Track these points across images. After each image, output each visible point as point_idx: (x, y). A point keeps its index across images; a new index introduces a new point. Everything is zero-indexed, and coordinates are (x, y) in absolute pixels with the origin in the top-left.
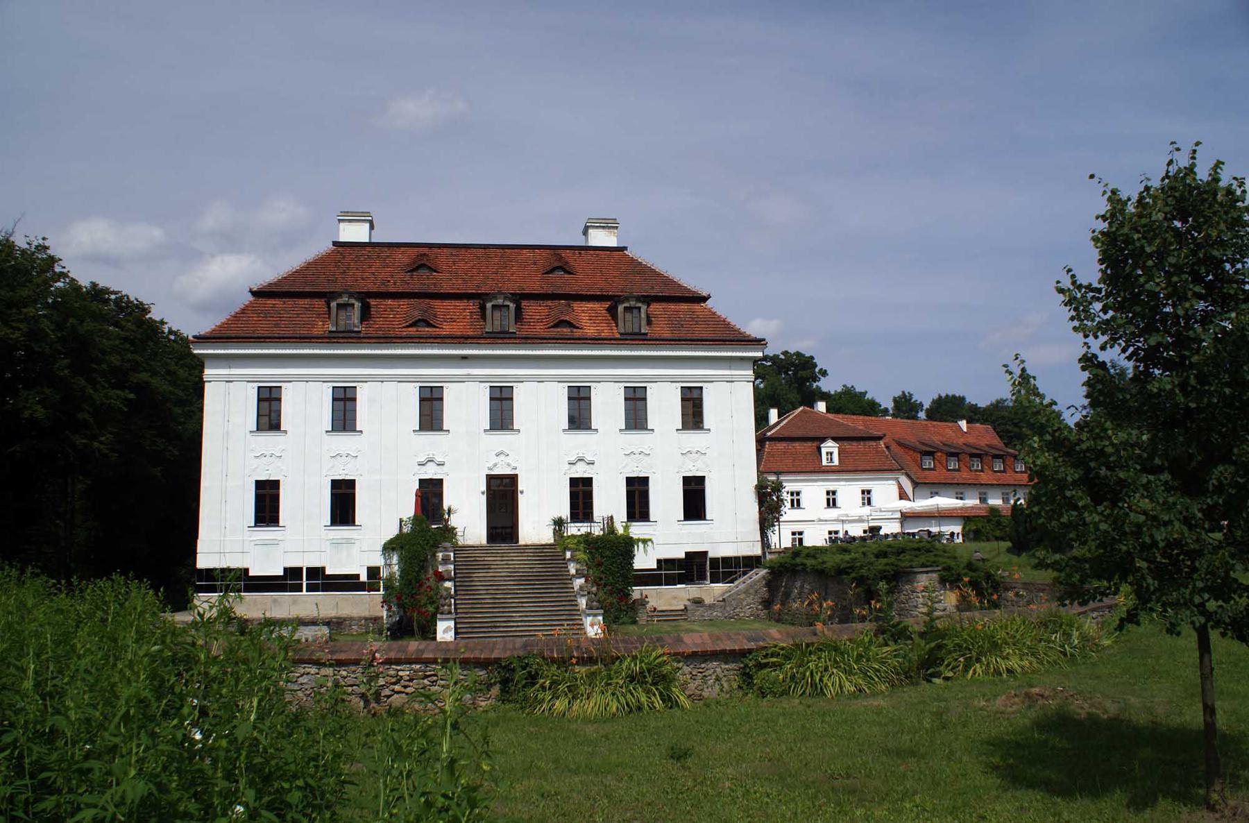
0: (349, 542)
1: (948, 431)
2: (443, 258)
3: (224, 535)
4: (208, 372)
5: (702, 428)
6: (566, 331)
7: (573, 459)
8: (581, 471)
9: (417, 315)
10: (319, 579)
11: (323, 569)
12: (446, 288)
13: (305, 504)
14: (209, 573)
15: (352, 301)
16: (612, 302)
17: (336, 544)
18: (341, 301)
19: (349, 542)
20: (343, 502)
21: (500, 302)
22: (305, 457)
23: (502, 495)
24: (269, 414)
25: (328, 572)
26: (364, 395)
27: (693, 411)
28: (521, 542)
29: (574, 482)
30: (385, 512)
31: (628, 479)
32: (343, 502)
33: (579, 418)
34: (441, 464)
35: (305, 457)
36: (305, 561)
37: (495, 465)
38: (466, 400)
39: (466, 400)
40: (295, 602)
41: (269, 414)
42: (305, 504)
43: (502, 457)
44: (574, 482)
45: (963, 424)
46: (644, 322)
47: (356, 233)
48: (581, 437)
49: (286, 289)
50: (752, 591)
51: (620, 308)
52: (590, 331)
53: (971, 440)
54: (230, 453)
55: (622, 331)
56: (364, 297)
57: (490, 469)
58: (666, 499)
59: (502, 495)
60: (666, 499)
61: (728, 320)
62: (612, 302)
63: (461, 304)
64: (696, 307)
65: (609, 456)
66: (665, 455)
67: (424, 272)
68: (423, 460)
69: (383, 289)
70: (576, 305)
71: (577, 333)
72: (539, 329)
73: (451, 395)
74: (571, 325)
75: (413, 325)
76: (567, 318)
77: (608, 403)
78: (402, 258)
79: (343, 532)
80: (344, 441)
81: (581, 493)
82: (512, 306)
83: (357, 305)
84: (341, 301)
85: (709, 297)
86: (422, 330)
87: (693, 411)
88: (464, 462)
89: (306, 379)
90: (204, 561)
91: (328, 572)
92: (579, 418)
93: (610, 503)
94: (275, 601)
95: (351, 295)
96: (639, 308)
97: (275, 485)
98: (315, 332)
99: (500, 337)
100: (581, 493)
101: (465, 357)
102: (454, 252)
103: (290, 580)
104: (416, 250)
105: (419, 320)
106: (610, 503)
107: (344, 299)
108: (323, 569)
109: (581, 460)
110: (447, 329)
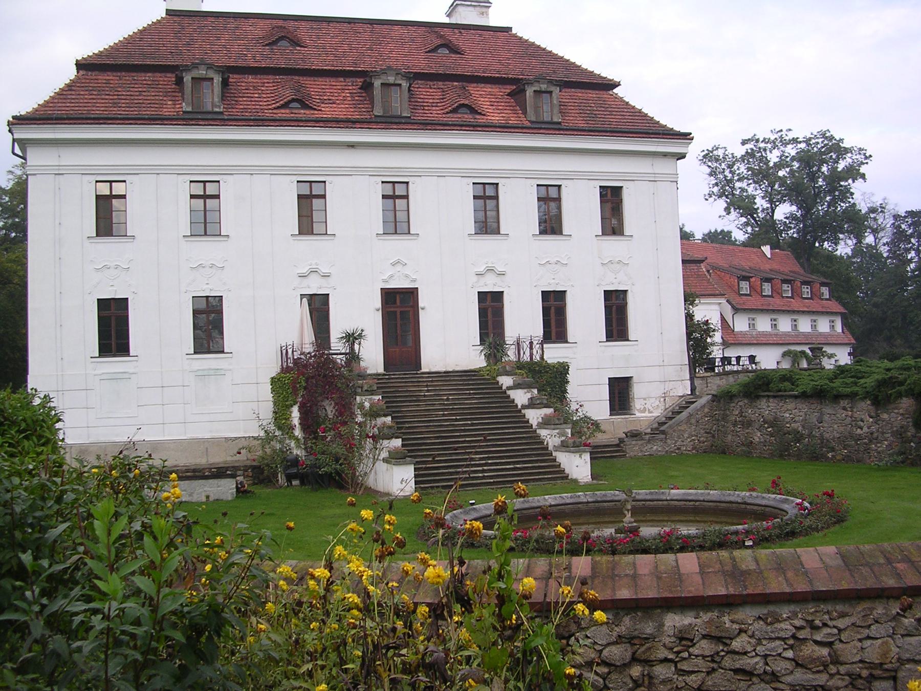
0: (218, 373)
1: (753, 256)
2: (303, 31)
5: (623, 235)
7: (482, 269)
8: (490, 285)
9: (288, 94)
12: (316, 64)
15: (211, 74)
16: (516, 88)
17: (202, 376)
18: (196, 73)
19: (218, 373)
20: (209, 325)
21: (391, 79)
24: (107, 217)
26: (229, 189)
28: (424, 370)
29: (482, 296)
30: (267, 332)
31: (544, 293)
32: (209, 325)
34: (326, 276)
37: (391, 276)
38: (354, 201)
39: (354, 201)
41: (107, 217)
42: (163, 327)
43: (399, 267)
45: (766, 249)
46: (556, 111)
48: (488, 242)
49: (121, 61)
50: (693, 421)
51: (529, 92)
52: (495, 118)
53: (775, 266)
57: (385, 281)
58: (585, 317)
60: (585, 317)
61: (645, 111)
62: (516, 88)
63: (339, 83)
64: (604, 95)
65: (523, 266)
68: (304, 270)
69: (241, 63)
70: (472, 88)
71: (481, 120)
72: (435, 114)
73: (335, 190)
74: (473, 111)
75: (285, 106)
76: (467, 102)
77: (519, 207)
78: (259, 30)
79: (209, 361)
80: (206, 249)
81: (491, 307)
82: (405, 84)
83: (217, 79)
84: (196, 73)
85: (617, 85)
86: (298, 111)
88: (355, 276)
89: (441, 174)
93: (523, 322)
95: (210, 67)
96: (551, 93)
97: (123, 303)
98: (166, 112)
99: (390, 122)
100: (491, 307)
101: (352, 146)
102: (115, 112)
104: (268, 22)
105: (293, 100)
106: (523, 322)
107: (202, 72)
109: (490, 270)
110: (327, 112)
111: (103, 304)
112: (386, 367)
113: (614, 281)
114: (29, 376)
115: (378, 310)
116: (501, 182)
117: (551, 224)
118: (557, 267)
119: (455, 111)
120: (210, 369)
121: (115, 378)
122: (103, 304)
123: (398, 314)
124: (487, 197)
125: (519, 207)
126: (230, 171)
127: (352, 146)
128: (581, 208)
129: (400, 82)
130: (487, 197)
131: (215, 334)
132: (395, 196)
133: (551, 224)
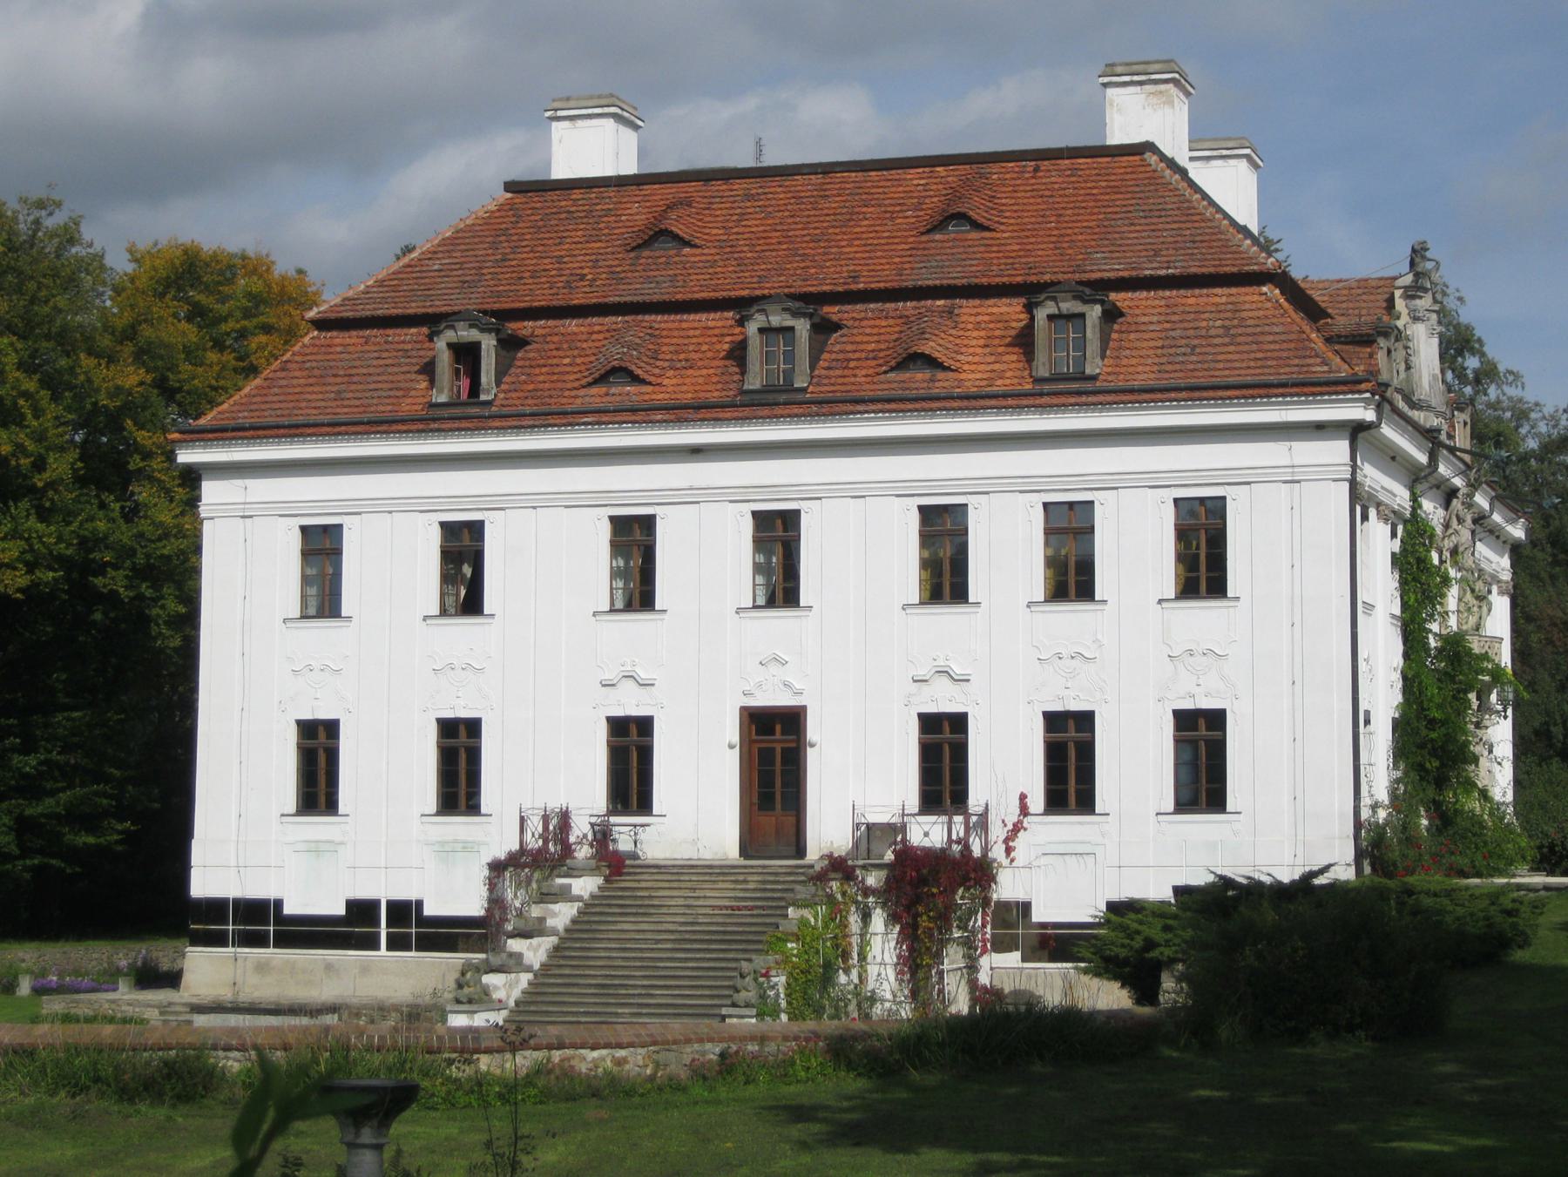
3: (240, 837)
4: (212, 492)
5: (966, 601)
6: (918, 378)
10: (411, 926)
11: (279, 904)
13: (389, 768)
14: (215, 908)
19: (334, 846)
22: (389, 669)
23: (774, 748)
25: (288, 910)
27: (1202, 563)
29: (929, 723)
31: (1176, 713)
33: (946, 577)
35: (389, 669)
36: (383, 889)
40: (365, 969)
42: (389, 768)
43: (774, 669)
44: (929, 723)
47: (589, 149)
52: (972, 379)
54: (251, 670)
55: (1043, 372)
56: (808, 302)
59: (774, 748)
65: (1008, 661)
66: (1135, 657)
67: (663, 252)
71: (944, 382)
72: (862, 380)
74: (932, 363)
77: (1008, 550)
87: (1202, 563)
89: (858, 492)
90: (204, 882)
91: (288, 910)
92: (946, 577)
94: (329, 967)
96: (1082, 316)
97: (1085, 720)
99: (775, 400)
103: (355, 925)
108: (279, 904)
110: (672, 387)
111: (1054, 721)
112: (745, 851)
113: (1196, 690)
114: (194, 842)
115: (731, 747)
116: (970, 500)
117: (1071, 578)
118: (1077, 663)
119: (602, 379)
120: (456, 841)
121: (316, 849)
122: (1054, 721)
123: (1071, 746)
124: (634, 540)
125: (1008, 550)
126: (499, 505)
127: (696, 452)
128: (1135, 549)
129: (789, 323)
130: (634, 540)
131: (1521, 777)
132: (778, 536)
133: (1071, 578)
